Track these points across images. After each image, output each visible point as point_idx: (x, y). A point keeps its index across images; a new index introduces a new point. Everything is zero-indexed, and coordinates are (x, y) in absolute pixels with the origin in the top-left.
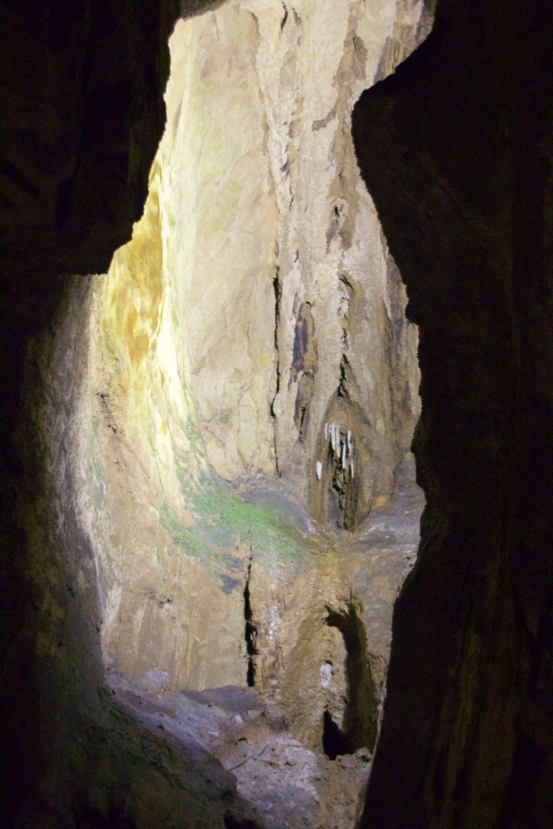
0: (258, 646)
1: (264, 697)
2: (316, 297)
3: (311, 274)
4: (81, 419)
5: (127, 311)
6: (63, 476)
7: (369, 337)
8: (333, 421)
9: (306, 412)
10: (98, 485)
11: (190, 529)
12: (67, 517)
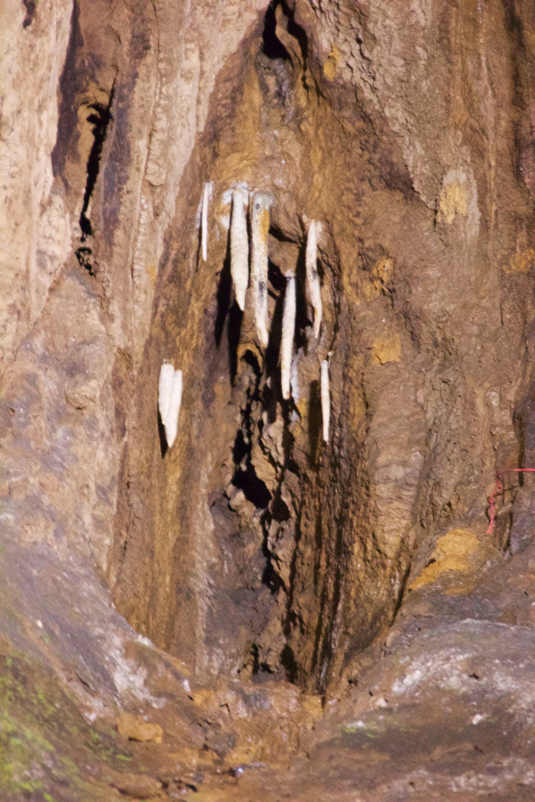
8: (238, 174)
9: (111, 132)
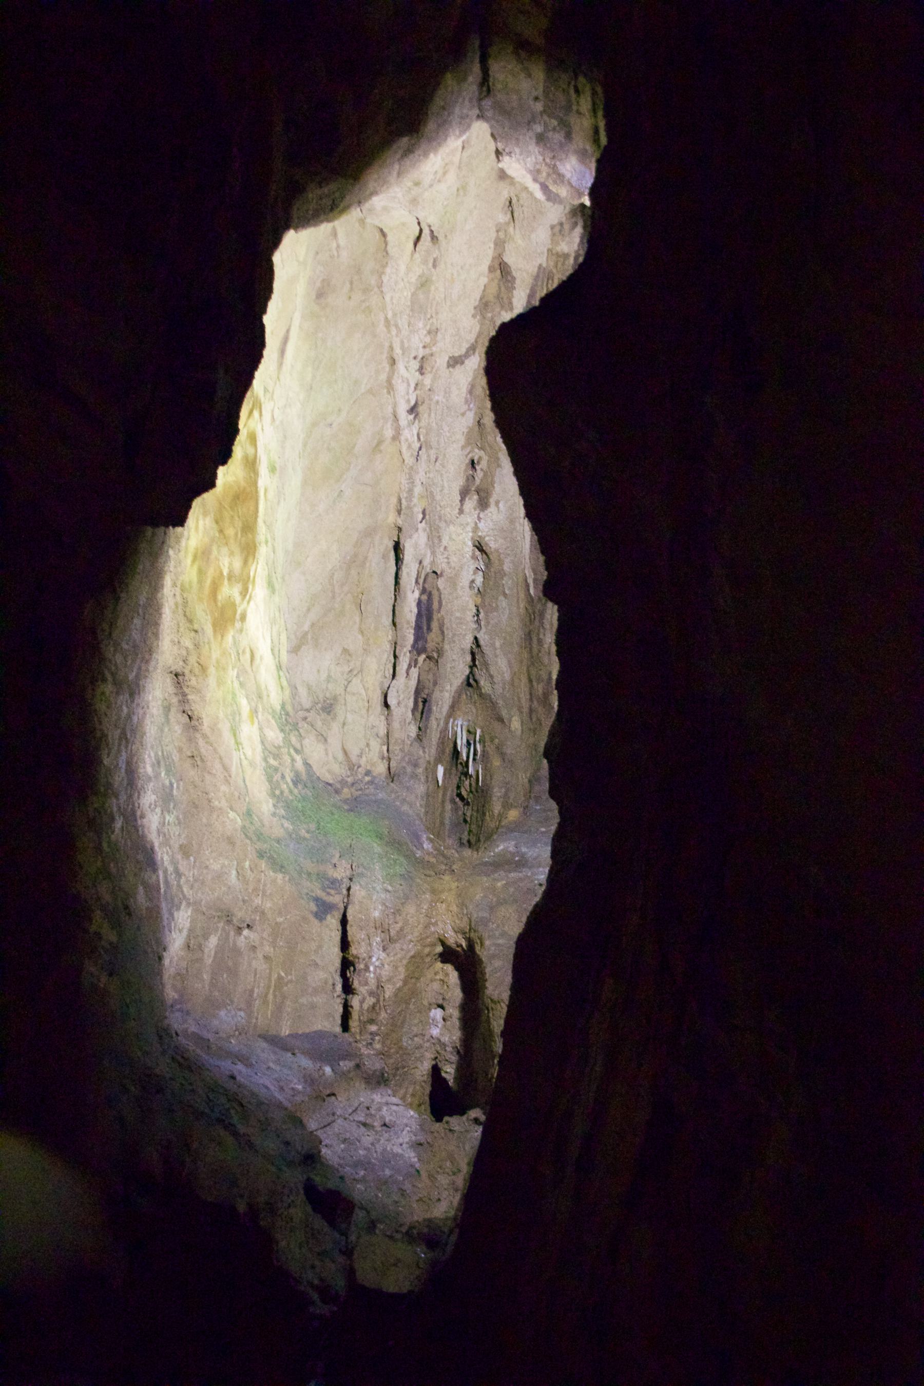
0: (356, 984)
1: (360, 1045)
2: (444, 565)
4: (148, 702)
5: (211, 573)
6: (123, 771)
9: (427, 705)
10: (167, 783)
11: (278, 841)
12: (126, 821)
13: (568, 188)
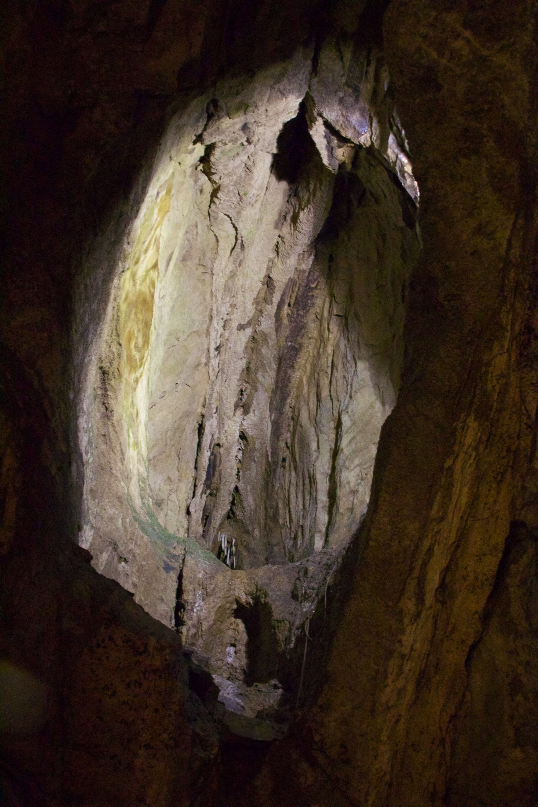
2: (224, 441)
3: (223, 425)
7: (254, 473)
13: (353, 131)
